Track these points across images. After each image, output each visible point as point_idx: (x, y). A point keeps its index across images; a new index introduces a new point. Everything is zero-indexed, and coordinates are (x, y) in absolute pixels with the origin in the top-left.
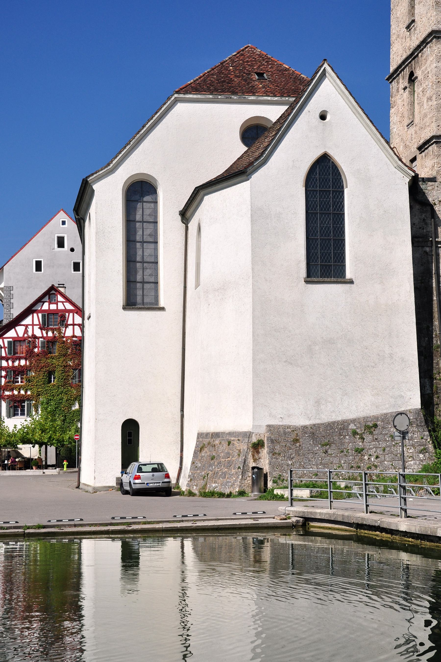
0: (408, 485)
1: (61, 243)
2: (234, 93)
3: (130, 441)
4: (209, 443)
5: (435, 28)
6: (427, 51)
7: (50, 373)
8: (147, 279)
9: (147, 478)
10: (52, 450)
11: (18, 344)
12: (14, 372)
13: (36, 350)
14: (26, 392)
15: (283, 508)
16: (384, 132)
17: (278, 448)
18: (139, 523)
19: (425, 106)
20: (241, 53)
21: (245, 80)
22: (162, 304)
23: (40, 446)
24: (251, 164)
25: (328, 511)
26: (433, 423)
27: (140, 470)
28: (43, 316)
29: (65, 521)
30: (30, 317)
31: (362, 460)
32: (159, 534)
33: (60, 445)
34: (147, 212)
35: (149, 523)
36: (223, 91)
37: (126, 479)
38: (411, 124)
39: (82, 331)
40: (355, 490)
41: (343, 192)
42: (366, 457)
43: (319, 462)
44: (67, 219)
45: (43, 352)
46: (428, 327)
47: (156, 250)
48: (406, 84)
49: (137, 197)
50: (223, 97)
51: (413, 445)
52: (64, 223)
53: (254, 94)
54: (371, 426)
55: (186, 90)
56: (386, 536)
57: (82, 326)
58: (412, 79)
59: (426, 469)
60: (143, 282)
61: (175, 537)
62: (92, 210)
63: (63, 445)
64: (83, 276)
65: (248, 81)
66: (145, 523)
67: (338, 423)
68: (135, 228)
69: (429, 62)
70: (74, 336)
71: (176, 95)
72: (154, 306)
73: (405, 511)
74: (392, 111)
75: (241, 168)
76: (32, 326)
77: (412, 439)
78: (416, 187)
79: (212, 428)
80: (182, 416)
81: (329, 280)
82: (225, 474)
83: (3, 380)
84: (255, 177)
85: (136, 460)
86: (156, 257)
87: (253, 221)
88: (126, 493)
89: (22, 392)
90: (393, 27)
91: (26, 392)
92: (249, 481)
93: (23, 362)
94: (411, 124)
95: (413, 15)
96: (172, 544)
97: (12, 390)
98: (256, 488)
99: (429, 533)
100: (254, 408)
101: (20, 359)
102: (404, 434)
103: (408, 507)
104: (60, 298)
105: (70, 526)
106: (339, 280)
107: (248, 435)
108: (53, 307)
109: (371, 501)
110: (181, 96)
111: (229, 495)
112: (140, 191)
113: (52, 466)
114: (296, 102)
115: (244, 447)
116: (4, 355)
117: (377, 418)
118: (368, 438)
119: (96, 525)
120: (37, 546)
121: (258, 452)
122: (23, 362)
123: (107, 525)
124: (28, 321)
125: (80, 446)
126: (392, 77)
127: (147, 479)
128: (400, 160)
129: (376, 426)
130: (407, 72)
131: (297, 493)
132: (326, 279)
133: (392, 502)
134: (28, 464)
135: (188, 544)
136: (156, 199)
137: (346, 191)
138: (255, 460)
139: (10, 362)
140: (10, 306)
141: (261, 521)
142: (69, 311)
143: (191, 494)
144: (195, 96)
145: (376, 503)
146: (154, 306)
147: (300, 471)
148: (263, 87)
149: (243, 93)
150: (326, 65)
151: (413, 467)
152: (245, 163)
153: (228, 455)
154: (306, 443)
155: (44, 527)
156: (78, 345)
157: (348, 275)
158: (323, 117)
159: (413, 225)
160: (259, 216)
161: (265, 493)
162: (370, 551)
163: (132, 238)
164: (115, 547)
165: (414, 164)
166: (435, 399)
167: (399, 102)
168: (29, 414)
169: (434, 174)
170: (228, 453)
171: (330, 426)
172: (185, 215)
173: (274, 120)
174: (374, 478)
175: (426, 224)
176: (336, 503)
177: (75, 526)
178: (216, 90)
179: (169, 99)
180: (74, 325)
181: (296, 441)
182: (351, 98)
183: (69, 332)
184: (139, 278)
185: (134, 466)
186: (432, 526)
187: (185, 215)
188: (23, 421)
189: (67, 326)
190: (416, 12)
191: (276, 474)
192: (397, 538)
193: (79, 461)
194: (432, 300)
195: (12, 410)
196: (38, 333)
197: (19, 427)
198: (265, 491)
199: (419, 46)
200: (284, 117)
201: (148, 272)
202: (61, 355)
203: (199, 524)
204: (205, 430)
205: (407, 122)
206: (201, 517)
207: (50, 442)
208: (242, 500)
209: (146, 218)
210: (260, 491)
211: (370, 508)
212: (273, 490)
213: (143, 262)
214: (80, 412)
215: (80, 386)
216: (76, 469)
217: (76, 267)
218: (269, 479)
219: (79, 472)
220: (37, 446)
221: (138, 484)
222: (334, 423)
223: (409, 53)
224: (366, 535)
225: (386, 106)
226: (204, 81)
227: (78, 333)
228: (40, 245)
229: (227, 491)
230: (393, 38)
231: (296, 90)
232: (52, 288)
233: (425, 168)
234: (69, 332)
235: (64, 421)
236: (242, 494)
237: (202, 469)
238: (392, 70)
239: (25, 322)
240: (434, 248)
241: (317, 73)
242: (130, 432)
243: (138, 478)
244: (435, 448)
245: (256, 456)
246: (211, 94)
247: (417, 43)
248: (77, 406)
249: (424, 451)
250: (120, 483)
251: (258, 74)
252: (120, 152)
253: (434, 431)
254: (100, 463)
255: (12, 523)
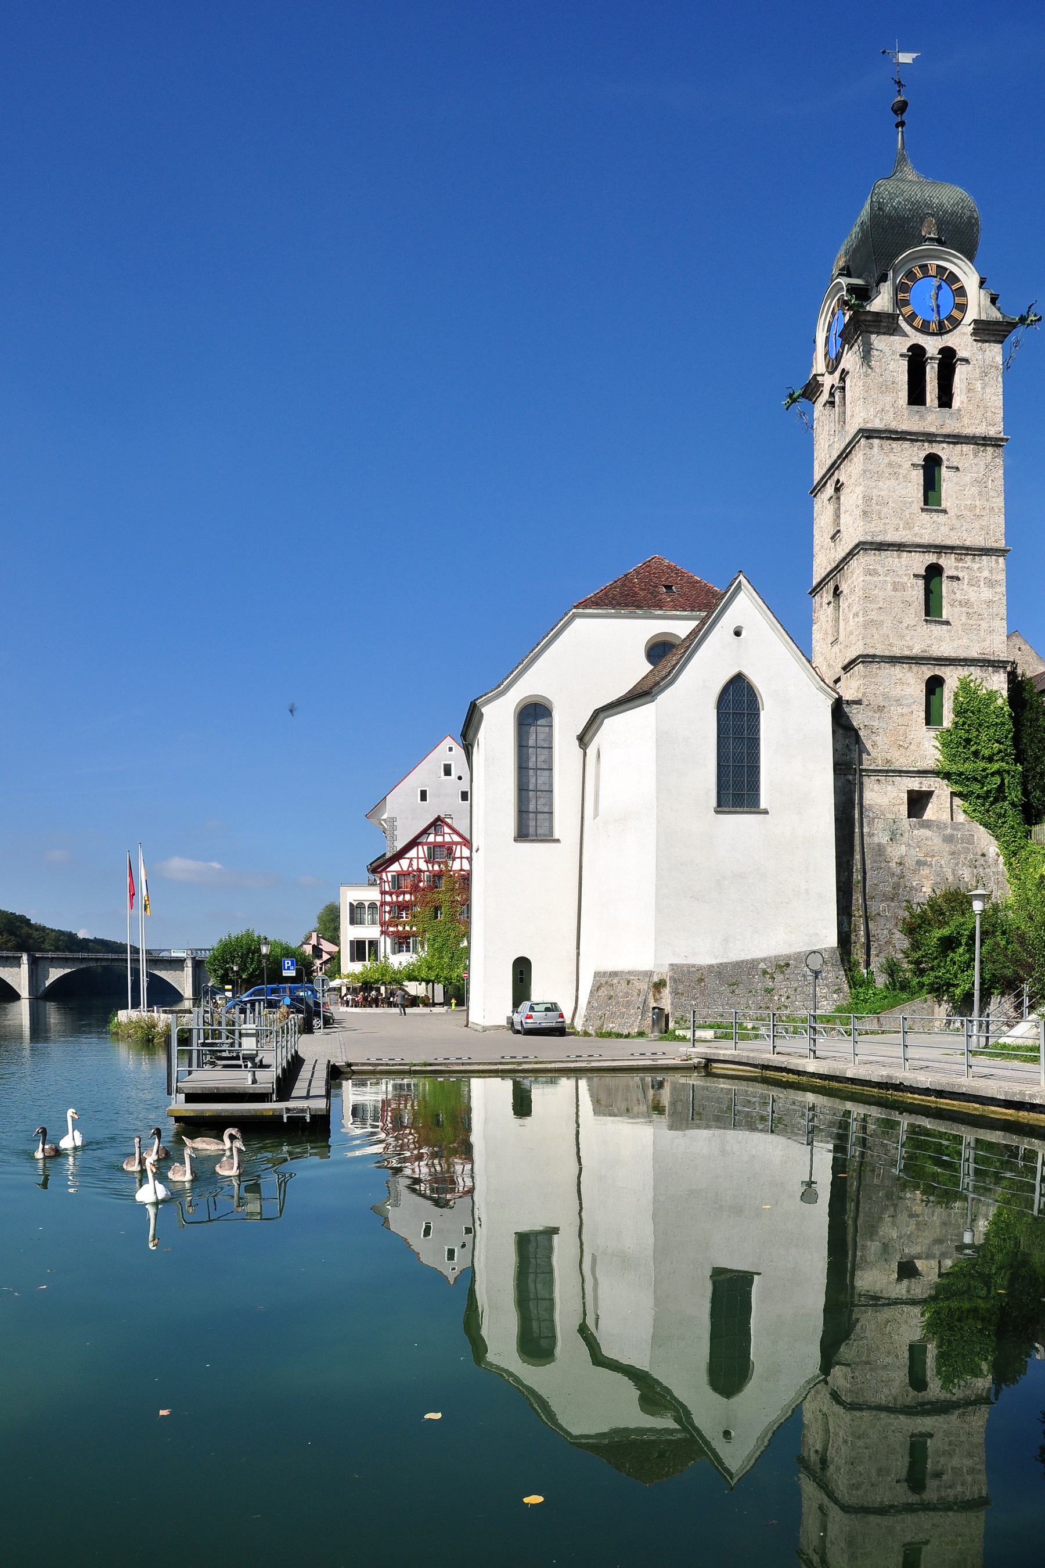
0: (818, 1026)
1: (447, 771)
2: (639, 607)
3: (522, 980)
4: (607, 983)
5: (862, 539)
6: (854, 563)
7: (437, 909)
8: (540, 808)
9: (540, 1018)
10: (439, 988)
11: (402, 878)
12: (399, 907)
13: (421, 884)
14: (411, 928)
15: (684, 1049)
16: (805, 650)
17: (681, 987)
18: (530, 1063)
19: (851, 623)
20: (647, 565)
21: (652, 593)
22: (557, 835)
23: (427, 984)
24: (657, 684)
25: (733, 1052)
26: (849, 962)
27: (532, 1009)
28: (429, 849)
29: (453, 1060)
30: (415, 849)
31: (771, 1000)
32: (553, 1074)
33: (448, 981)
34: (541, 736)
35: (541, 1063)
36: (627, 605)
37: (517, 1018)
38: (835, 642)
39: (471, 865)
40: (763, 1031)
41: (759, 715)
42: (776, 998)
43: (725, 1002)
44: (454, 745)
45: (430, 886)
46: (848, 861)
47: (551, 777)
48: (831, 598)
49: (530, 721)
50: (626, 611)
51: (827, 985)
52: (451, 749)
53: (661, 608)
54: (782, 965)
55: (585, 604)
56: (792, 1078)
57: (470, 859)
58: (837, 593)
59: (839, 1009)
60: (536, 812)
61: (568, 1078)
62: (481, 735)
63: (451, 983)
64: (471, 806)
65: (655, 594)
66: (536, 1063)
67: (747, 961)
68: (528, 797)
69: (855, 575)
70: (462, 870)
71: (574, 610)
72: (549, 838)
73: (815, 1052)
74: (815, 627)
75: (645, 688)
76: (417, 859)
77: (826, 978)
78: (839, 711)
79: (610, 967)
80: (578, 954)
81: (741, 809)
82: (623, 1014)
83: (387, 915)
84: (661, 698)
85: (529, 999)
86: (551, 785)
87: (658, 746)
88: (518, 1032)
89: (407, 928)
90: (816, 537)
91: (411, 928)
92: (649, 1021)
93: (407, 897)
94: (835, 642)
95: (838, 525)
96: (566, 1084)
97: (397, 926)
98: (656, 1028)
99: (838, 1074)
100: (656, 946)
101: (404, 893)
102: (816, 974)
103: (818, 1047)
104: (447, 830)
105: (458, 1064)
106: (753, 810)
107: (650, 974)
108: (439, 839)
109: (778, 1042)
110: (580, 611)
111: (627, 1036)
112: (534, 714)
113: (440, 1004)
114: (708, 617)
115: (644, 986)
116: (387, 889)
117: (789, 957)
118: (779, 977)
119: (485, 1064)
120: (425, 1085)
121: (659, 992)
122: (407, 897)
123: (496, 1064)
124: (412, 853)
125: (468, 984)
126: (815, 591)
127: (540, 1019)
128: (823, 681)
129: (788, 965)
130: (831, 585)
131: (700, 1033)
132: (738, 809)
133: (802, 1043)
134: (414, 1001)
135: (583, 1083)
136: (551, 722)
137: (762, 713)
138: (656, 1000)
139: (394, 897)
140: (394, 838)
141: (660, 1062)
142: (457, 843)
143: (586, 1034)
144: (595, 611)
145: (782, 1045)
146: (549, 838)
147: (704, 1012)
148: (672, 601)
149: (649, 607)
150: (741, 577)
151: (826, 1008)
152: (650, 682)
153: (627, 995)
154: (712, 982)
155: (430, 1065)
156: (466, 879)
157: (763, 805)
158: (738, 633)
159: (835, 751)
160: (663, 740)
161: (666, 1033)
162: (774, 1092)
163: (524, 765)
164: (506, 1086)
165: (838, 685)
166: (853, 937)
167: (823, 618)
168: (415, 951)
169: (860, 696)
170: (627, 993)
171: (738, 965)
172: (583, 739)
173: (683, 637)
174: (784, 1018)
175: (850, 750)
176: (741, 1044)
177: (463, 1064)
178: (619, 604)
179: (566, 614)
180: (461, 858)
181: (701, 980)
182: (769, 612)
183: (456, 866)
184: (532, 808)
185: (525, 1006)
186: (841, 1067)
187: (583, 739)
188: (408, 957)
189: (454, 859)
190: (841, 521)
191: (678, 1014)
192: (804, 1079)
193: (468, 999)
194: (854, 832)
195: (397, 946)
196: (423, 866)
197: (404, 964)
198: (666, 1032)
199: (844, 558)
200: (694, 633)
201: (541, 801)
202: (447, 890)
203: (594, 1064)
204: (602, 969)
205: (831, 639)
206: (596, 1057)
207: (438, 979)
208: (642, 1040)
209: (540, 743)
210: (661, 1032)
211: (777, 1049)
212: (674, 1031)
213: (536, 791)
214: (468, 949)
215: (468, 923)
216: (465, 1008)
217: (465, 796)
218: (670, 1019)
219: (468, 1010)
220: (424, 984)
221: (530, 1024)
222: (742, 962)
223: (834, 565)
224: (770, 1075)
225: (808, 623)
226: (606, 594)
227: (466, 866)
228: (426, 773)
229: (625, 1032)
230: (816, 549)
231: (707, 603)
232: (438, 819)
233: (849, 690)
234: (456, 866)
235: (452, 958)
236: (641, 1034)
237: (599, 1009)
238: (814, 583)
239: (409, 855)
240: (857, 776)
241: (731, 585)
242: (522, 969)
243: (530, 1017)
244: (850, 987)
245: (658, 996)
246: (613, 608)
247: (843, 555)
248: (465, 943)
249: (838, 991)
250: (511, 1023)
251: (666, 587)
252: (512, 673)
253: (850, 970)
254: (490, 1001)
255: (398, 1060)
